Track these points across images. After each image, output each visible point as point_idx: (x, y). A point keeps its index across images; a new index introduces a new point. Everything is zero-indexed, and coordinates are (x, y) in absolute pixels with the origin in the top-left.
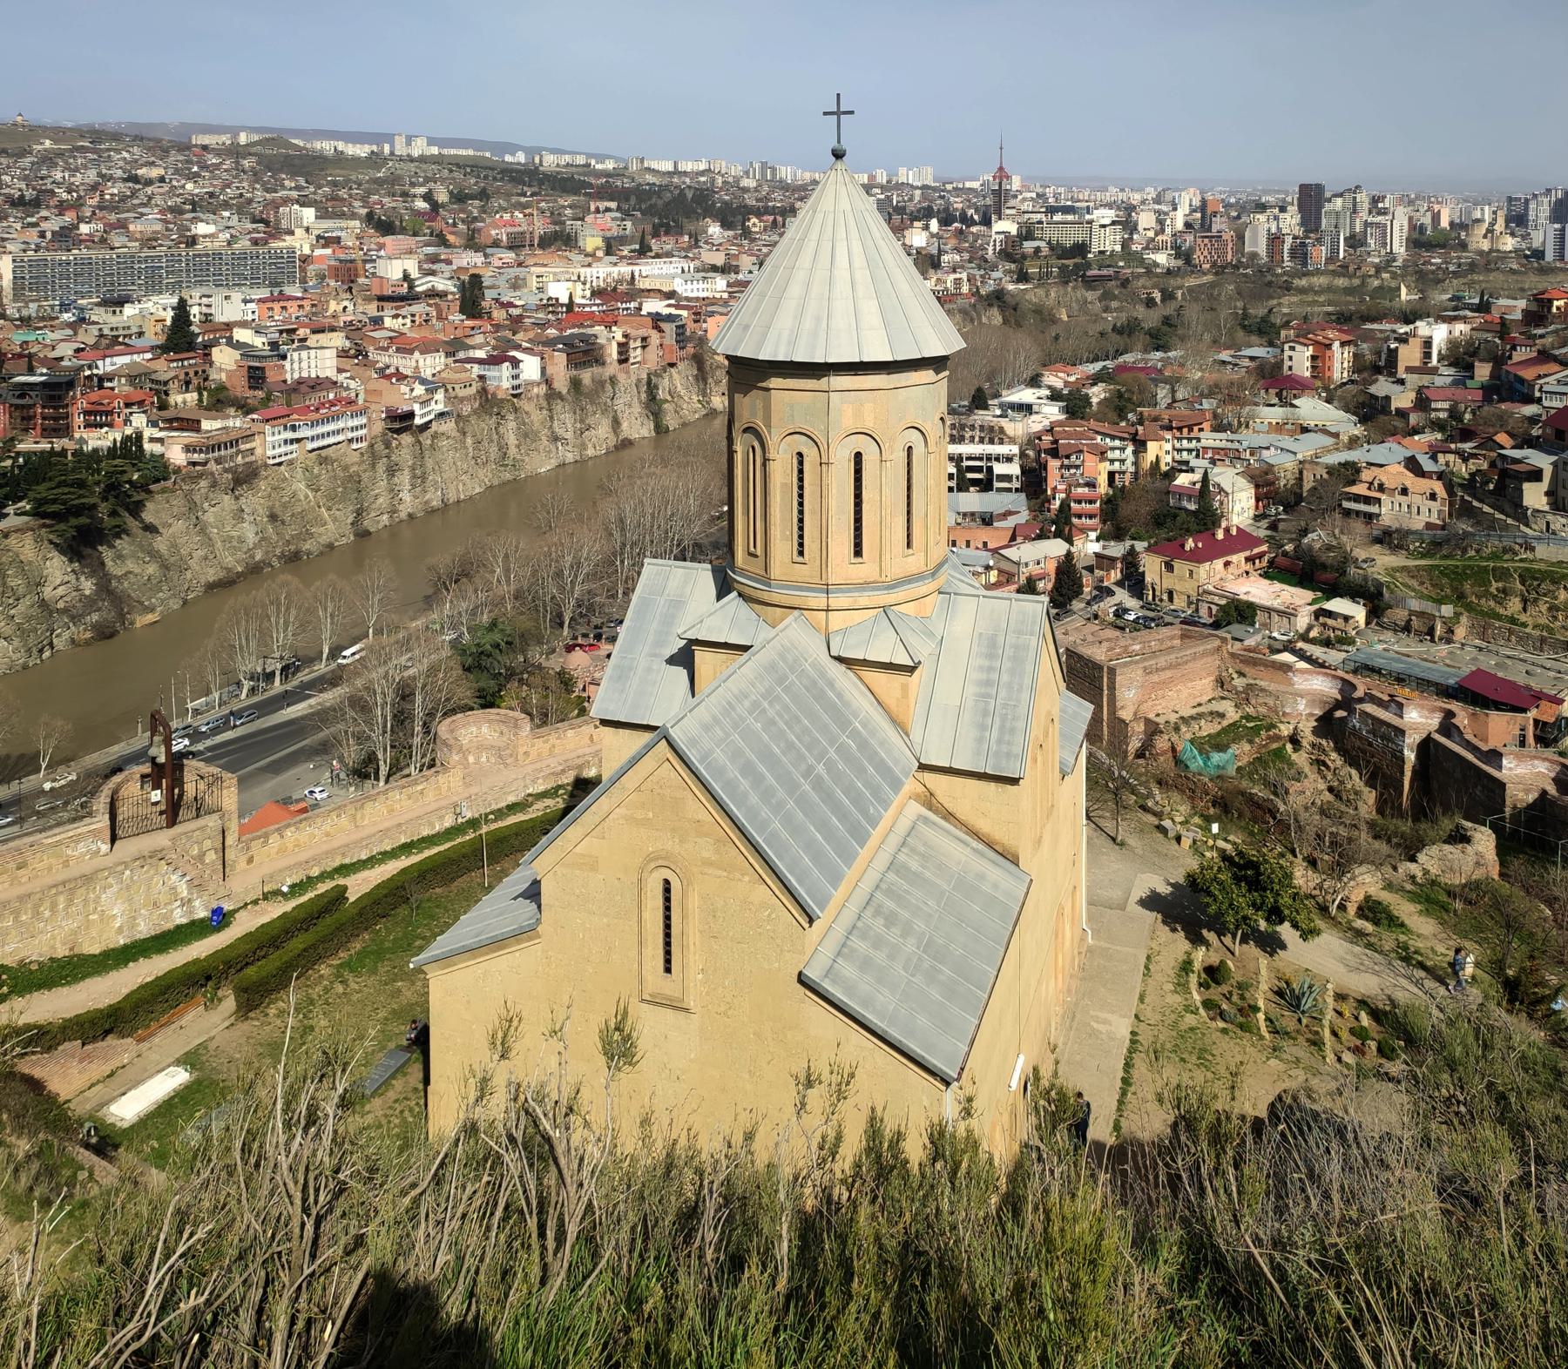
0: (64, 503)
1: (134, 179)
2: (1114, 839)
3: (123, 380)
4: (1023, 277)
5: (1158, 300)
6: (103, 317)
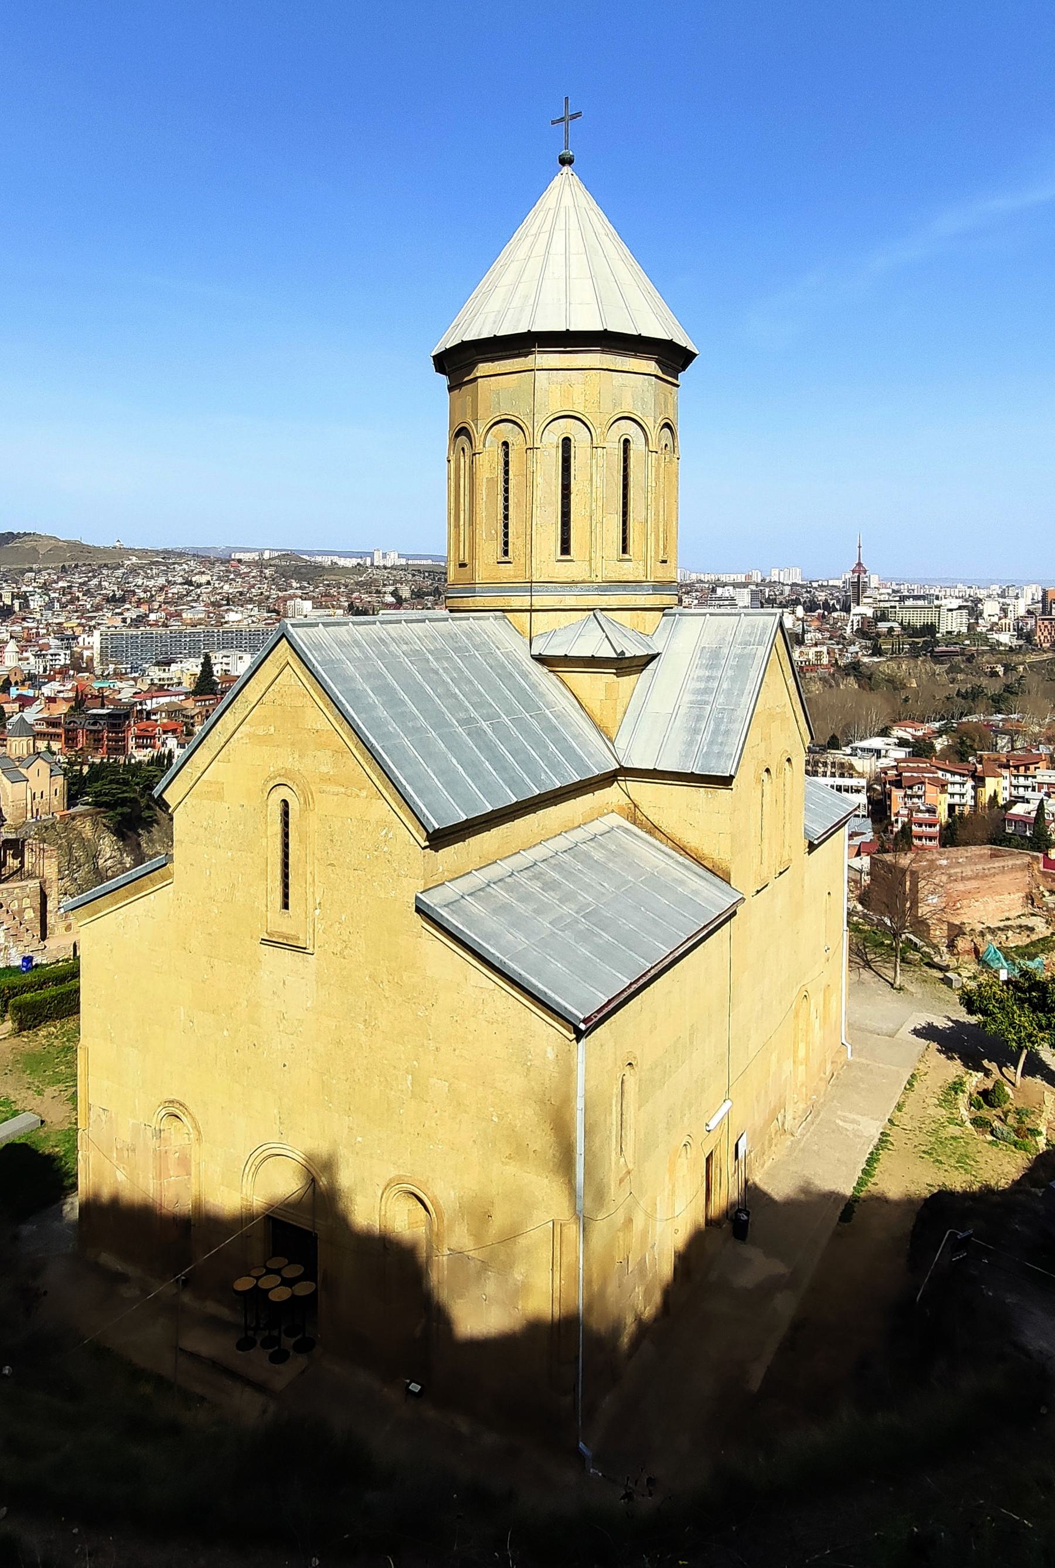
0: (114, 795)
1: (189, 583)
2: (892, 985)
3: (164, 714)
4: (877, 651)
5: (1001, 673)
6: (156, 673)
